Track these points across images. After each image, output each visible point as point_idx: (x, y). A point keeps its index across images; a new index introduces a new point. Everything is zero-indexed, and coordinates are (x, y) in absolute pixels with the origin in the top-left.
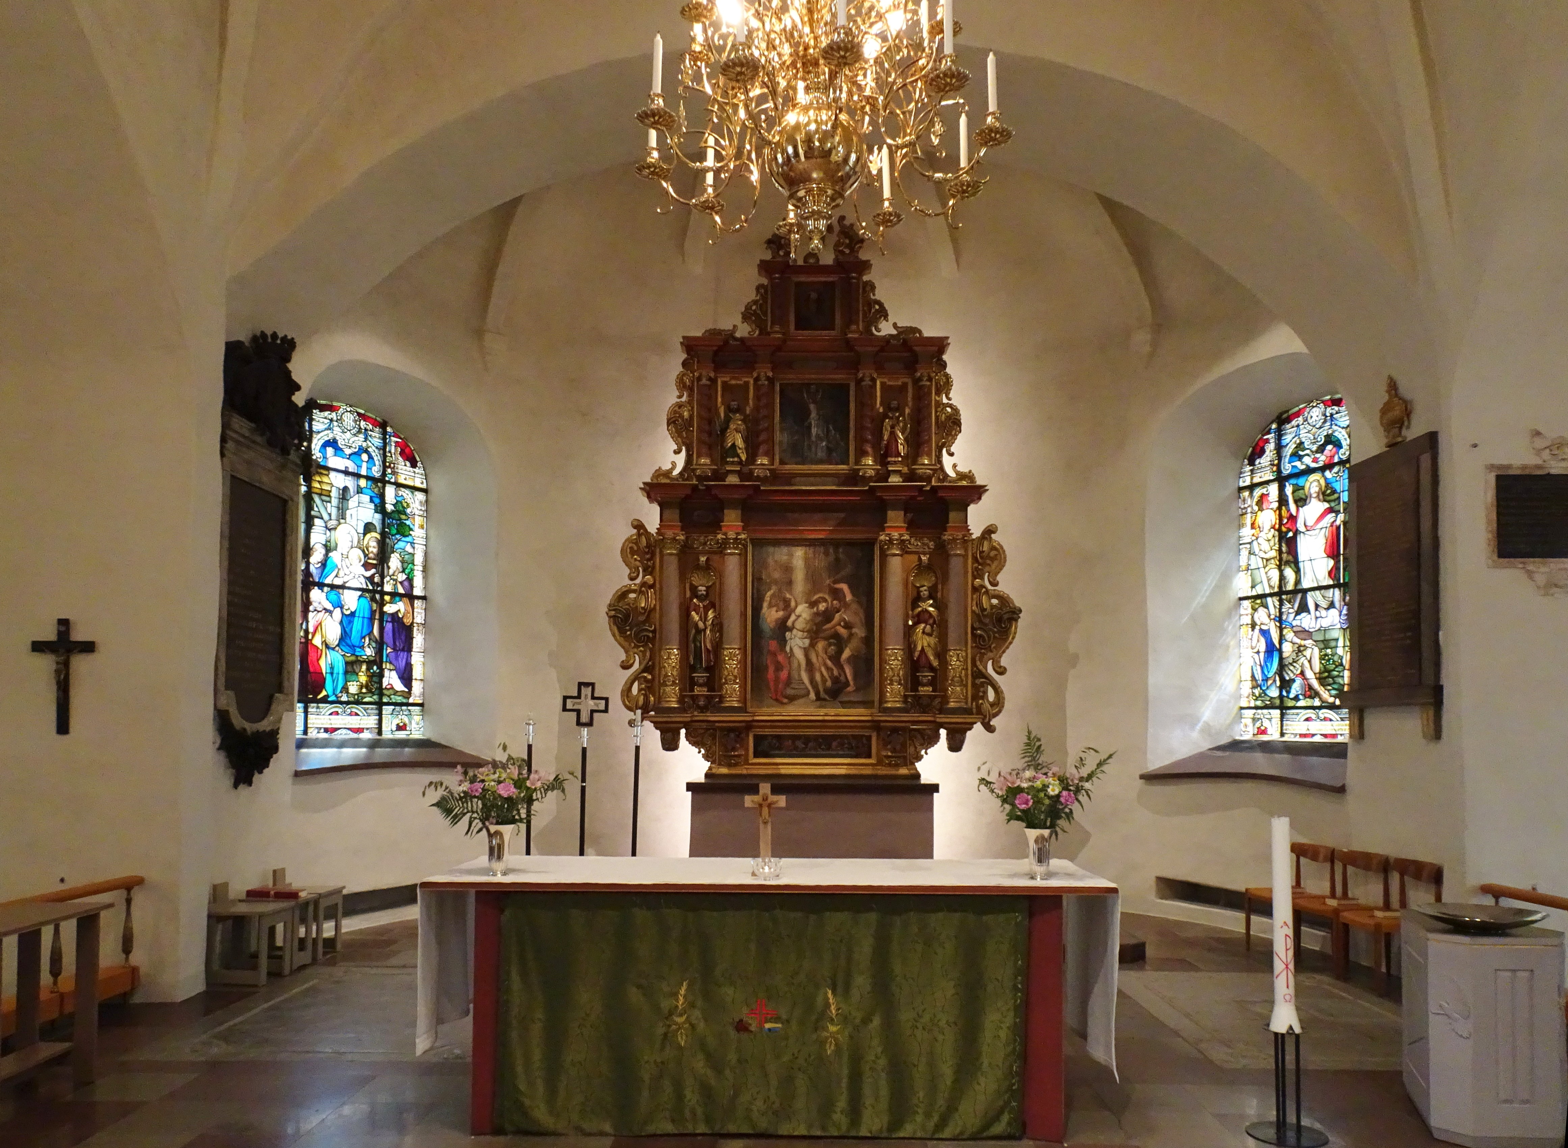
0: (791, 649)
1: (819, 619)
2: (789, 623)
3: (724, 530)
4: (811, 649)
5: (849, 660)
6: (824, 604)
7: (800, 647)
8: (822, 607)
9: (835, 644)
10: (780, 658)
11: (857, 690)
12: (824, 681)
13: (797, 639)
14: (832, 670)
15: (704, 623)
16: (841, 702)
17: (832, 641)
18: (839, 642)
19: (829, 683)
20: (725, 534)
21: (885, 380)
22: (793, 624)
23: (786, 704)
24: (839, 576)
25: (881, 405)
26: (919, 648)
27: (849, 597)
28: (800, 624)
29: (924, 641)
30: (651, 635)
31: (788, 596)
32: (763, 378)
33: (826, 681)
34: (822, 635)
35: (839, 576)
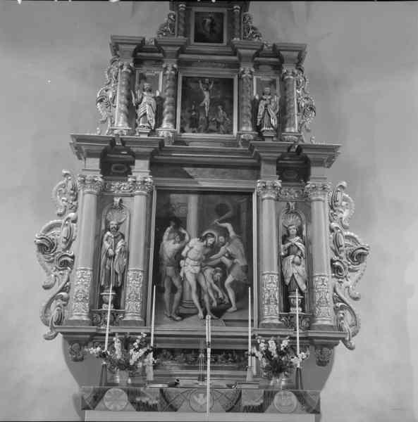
0: (184, 274)
1: (207, 250)
2: (184, 253)
3: (134, 174)
4: (201, 274)
5: (232, 284)
6: (212, 239)
7: (192, 273)
8: (210, 241)
9: (220, 272)
10: (176, 282)
11: (239, 309)
12: (211, 302)
13: (189, 266)
14: (217, 293)
15: (114, 251)
16: (224, 320)
17: (218, 268)
18: (225, 271)
19: (215, 304)
20: (135, 178)
21: (260, 77)
22: (187, 254)
23: (177, 321)
24: (223, 218)
25: (257, 93)
26: (291, 275)
27: (232, 234)
28: (192, 254)
29: (296, 270)
30: (69, 259)
31: (183, 231)
32: (170, 68)
33: (213, 301)
34: (210, 263)
35: (223, 218)
